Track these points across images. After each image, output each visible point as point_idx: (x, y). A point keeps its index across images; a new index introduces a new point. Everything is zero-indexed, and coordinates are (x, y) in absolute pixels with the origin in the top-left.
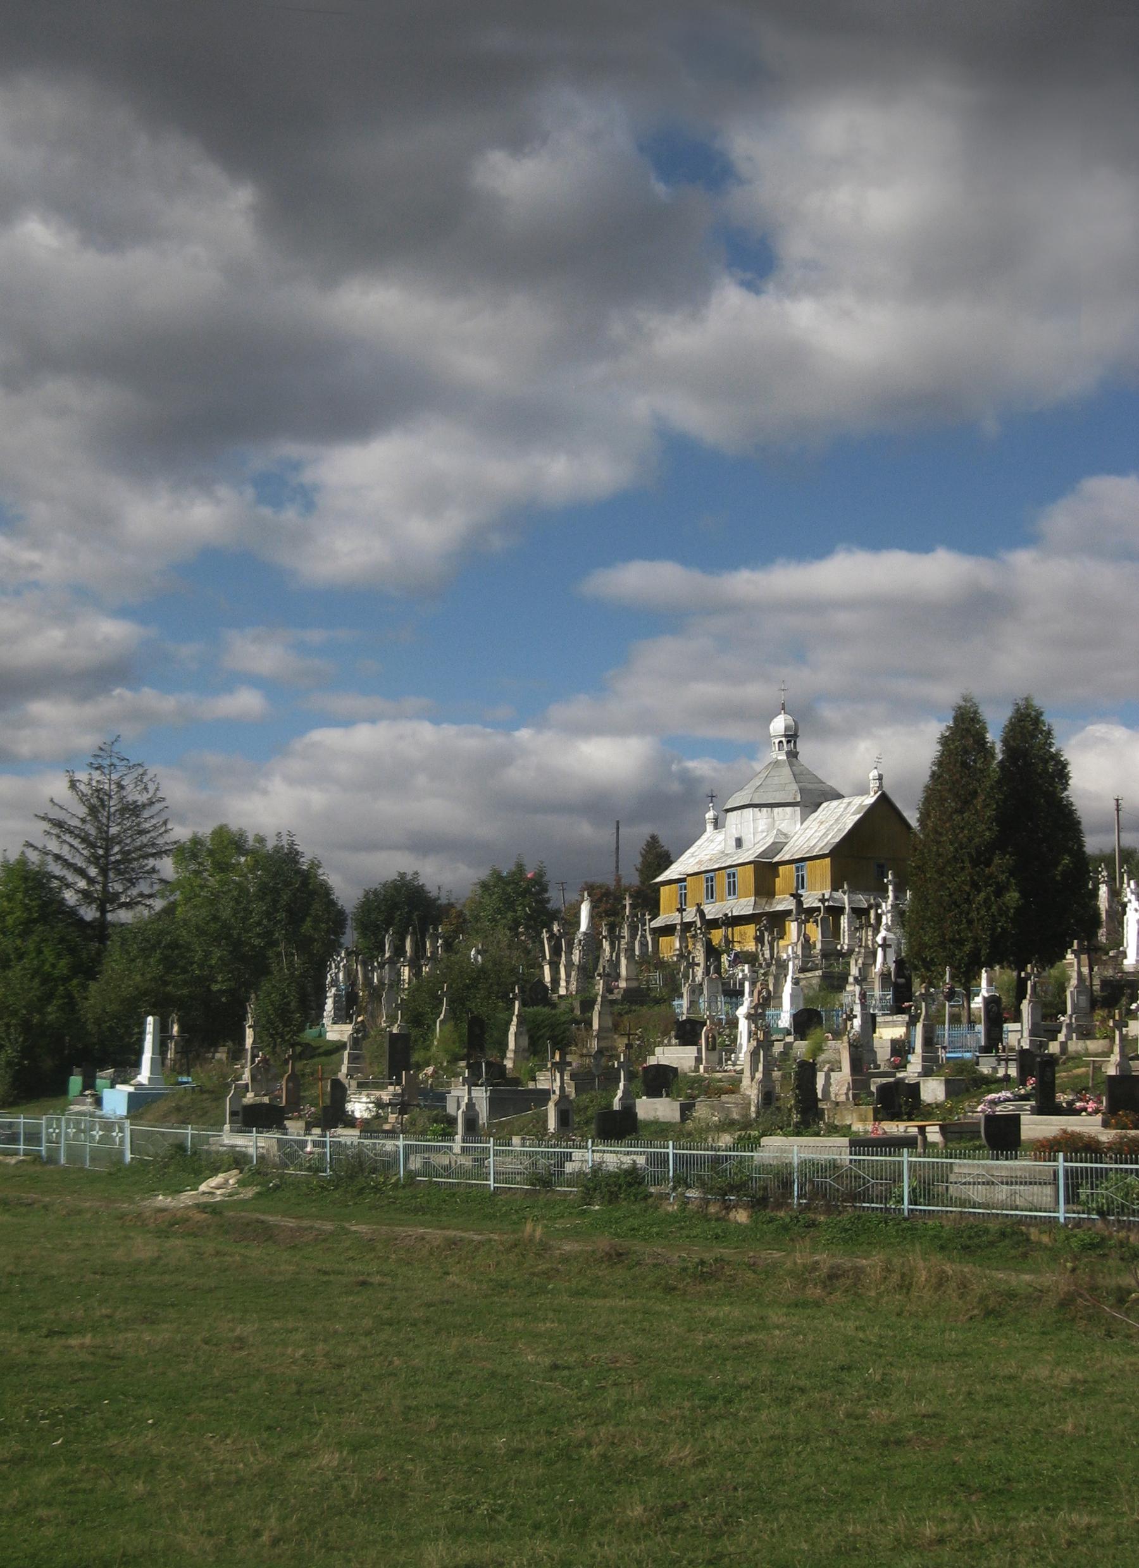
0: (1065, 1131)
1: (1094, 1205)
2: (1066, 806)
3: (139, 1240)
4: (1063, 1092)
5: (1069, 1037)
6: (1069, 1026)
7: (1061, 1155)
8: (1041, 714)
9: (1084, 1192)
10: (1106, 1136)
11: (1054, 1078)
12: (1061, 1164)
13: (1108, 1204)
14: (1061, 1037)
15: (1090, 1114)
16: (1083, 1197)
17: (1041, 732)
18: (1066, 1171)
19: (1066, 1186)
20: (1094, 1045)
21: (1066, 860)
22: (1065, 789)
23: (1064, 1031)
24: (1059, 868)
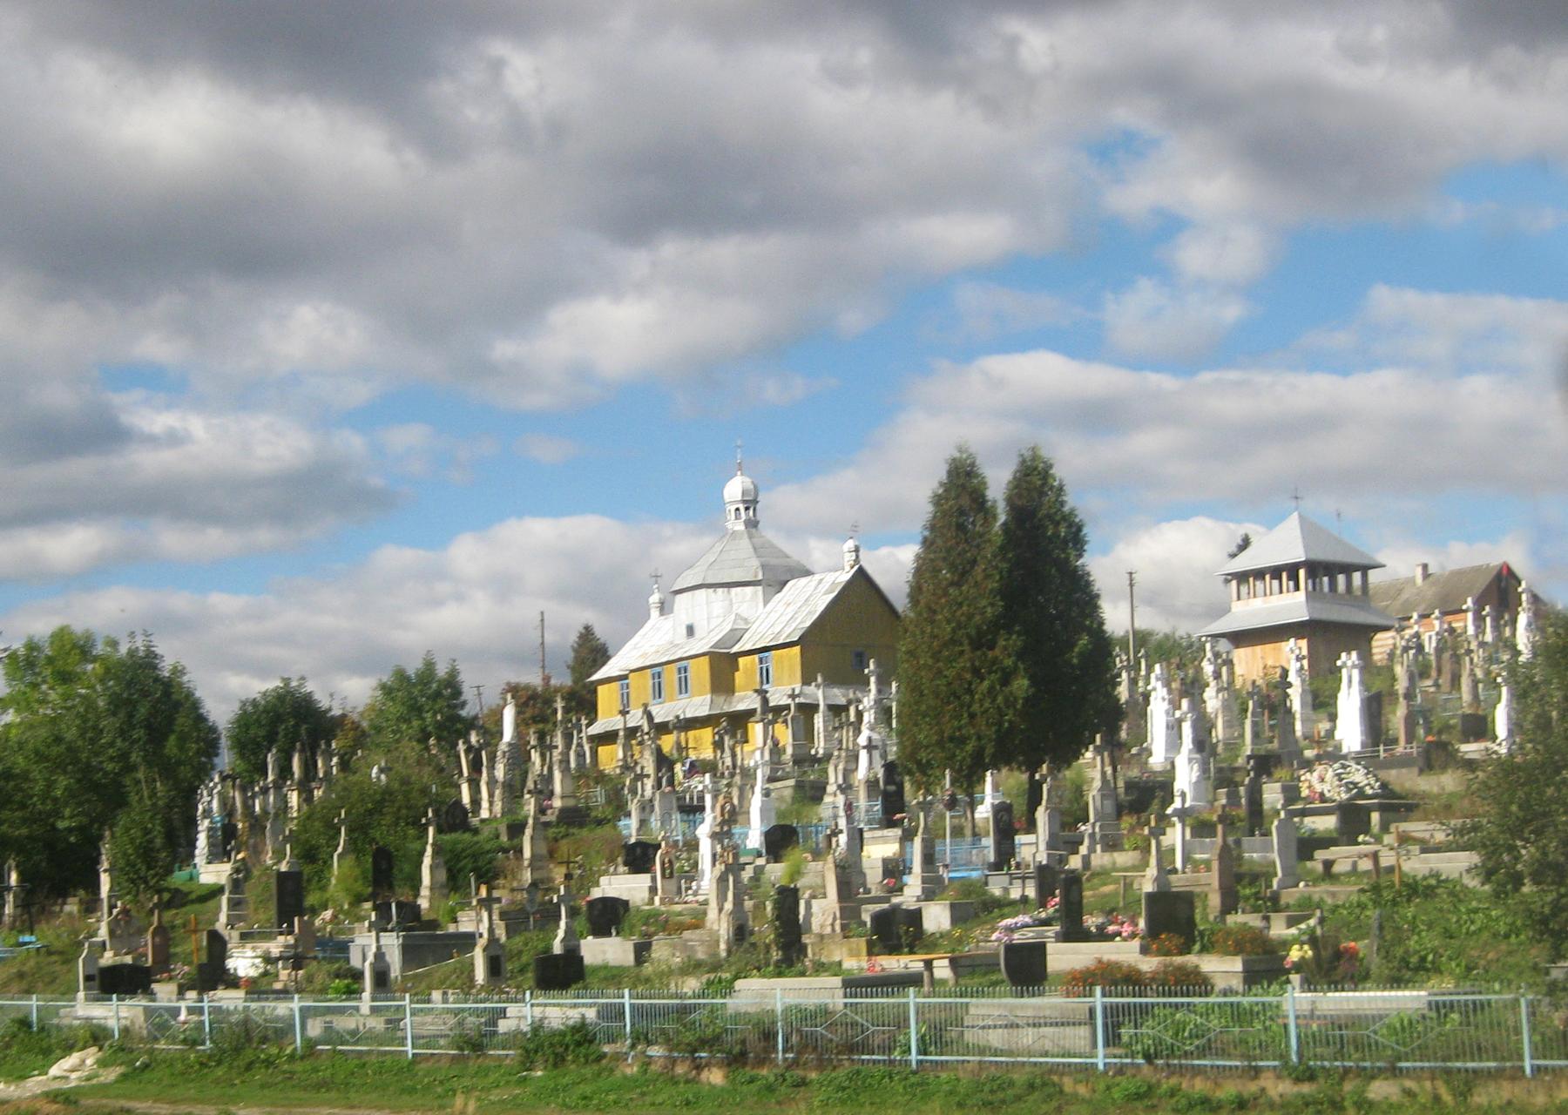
0: (1100, 961)
1: (1139, 1047)
5: (1092, 850)
7: (1098, 990)
8: (1051, 466)
9: (1126, 1032)
10: (1149, 964)
12: (1098, 999)
14: (1083, 850)
15: (1125, 940)
16: (1125, 1039)
17: (1052, 488)
18: (917, 1004)
19: (1105, 1025)
20: (1124, 858)
21: (1084, 640)
22: (1080, 556)
23: (1086, 842)
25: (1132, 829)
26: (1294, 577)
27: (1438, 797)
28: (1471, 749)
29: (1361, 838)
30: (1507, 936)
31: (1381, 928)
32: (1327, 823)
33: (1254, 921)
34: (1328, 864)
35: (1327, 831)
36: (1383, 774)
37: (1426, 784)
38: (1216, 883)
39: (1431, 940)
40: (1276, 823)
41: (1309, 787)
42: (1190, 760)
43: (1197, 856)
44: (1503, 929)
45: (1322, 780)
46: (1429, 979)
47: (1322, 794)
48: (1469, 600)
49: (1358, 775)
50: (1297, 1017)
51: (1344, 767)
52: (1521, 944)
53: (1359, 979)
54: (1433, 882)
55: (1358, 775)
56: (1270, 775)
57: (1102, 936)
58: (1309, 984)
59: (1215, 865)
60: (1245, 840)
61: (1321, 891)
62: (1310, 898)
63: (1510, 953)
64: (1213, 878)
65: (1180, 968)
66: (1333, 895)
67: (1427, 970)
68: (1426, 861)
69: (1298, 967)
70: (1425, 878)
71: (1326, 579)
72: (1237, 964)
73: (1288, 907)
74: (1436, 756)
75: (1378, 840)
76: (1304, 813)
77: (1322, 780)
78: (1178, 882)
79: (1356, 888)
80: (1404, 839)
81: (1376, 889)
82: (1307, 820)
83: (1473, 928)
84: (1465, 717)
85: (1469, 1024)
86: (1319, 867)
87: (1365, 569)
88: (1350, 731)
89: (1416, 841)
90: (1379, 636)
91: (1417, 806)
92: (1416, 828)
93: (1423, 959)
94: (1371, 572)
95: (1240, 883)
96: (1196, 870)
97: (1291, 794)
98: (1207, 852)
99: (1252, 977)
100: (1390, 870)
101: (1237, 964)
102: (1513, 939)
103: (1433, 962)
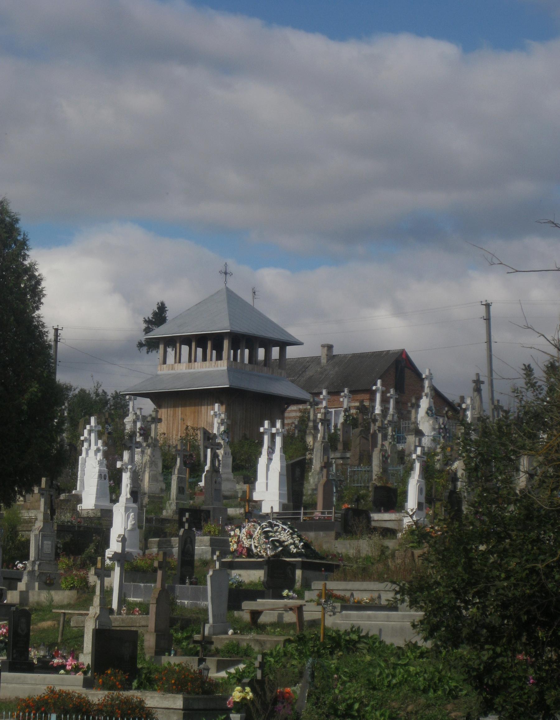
0: (52, 691)
3: (528, 591)
5: (29, 586)
6: (31, 573)
8: (17, 221)
14: (22, 586)
15: (68, 672)
17: (16, 241)
20: (61, 596)
21: (35, 388)
22: (38, 308)
23: (25, 579)
24: (26, 397)
25: (69, 569)
28: (381, 518)
29: (285, 593)
31: (313, 676)
32: (255, 576)
33: (192, 663)
34: (255, 614)
35: (251, 583)
36: (311, 536)
37: (344, 547)
38: (152, 625)
40: (211, 573)
41: (238, 542)
42: (127, 509)
43: (131, 599)
44: (421, 682)
45: (250, 536)
47: (249, 550)
48: (379, 382)
49: (284, 535)
52: (438, 698)
54: (354, 637)
55: (284, 535)
56: (199, 528)
57: (45, 667)
59: (153, 609)
60: (178, 586)
61: (248, 639)
62: (238, 645)
63: (428, 706)
64: (151, 620)
65: (127, 701)
68: (347, 617)
70: (347, 633)
71: (247, 351)
73: (217, 652)
74: (353, 522)
75: (301, 596)
76: (232, 566)
77: (250, 536)
78: (118, 621)
79: (282, 639)
80: (329, 596)
81: (301, 640)
82: (235, 573)
83: (394, 681)
86: (246, 617)
87: (283, 345)
88: (268, 490)
89: (342, 599)
90: (293, 408)
91: (338, 566)
92: (336, 586)
93: (350, 707)
94: (289, 348)
95: (176, 627)
97: (220, 544)
98: (146, 594)
100: (314, 623)
102: (431, 694)
103: (358, 711)
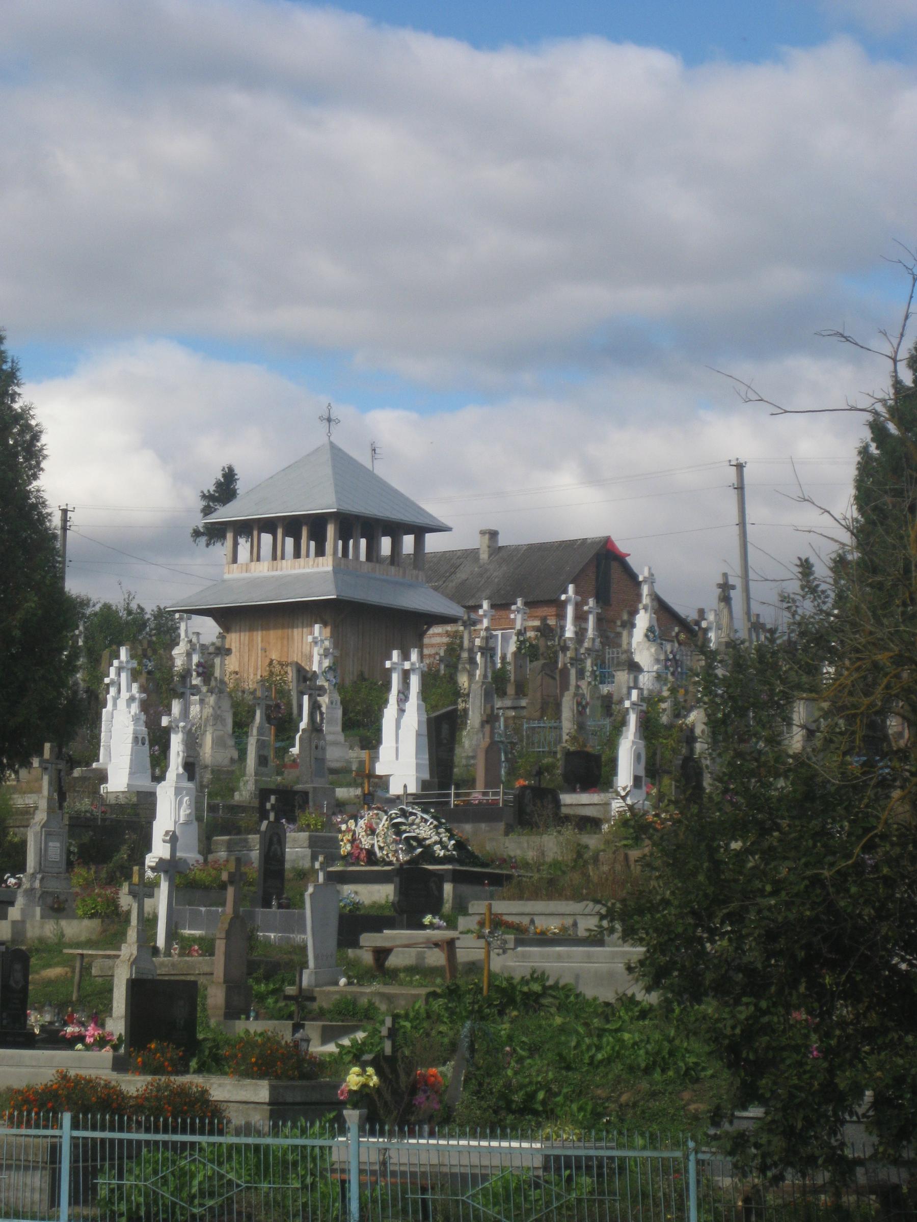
0: (64, 1077)
1: (124, 1207)
2: (34, 506)
4: (40, 1010)
7: (67, 1118)
9: (104, 1183)
10: (134, 1084)
11: (27, 982)
12: (66, 1131)
13: (147, 1205)
15: (88, 1047)
16: (103, 1193)
18: (74, 1140)
19: (74, 1171)
22: (35, 477)
23: (20, 901)
26: (319, 537)
27: (538, 866)
29: (427, 919)
30: (648, 1071)
33: (284, 1031)
34: (381, 954)
35: (374, 905)
37: (519, 847)
39: (540, 1070)
42: (178, 791)
43: (187, 932)
45: (371, 831)
46: (539, 1125)
47: (370, 853)
50: (361, 1172)
51: (404, 813)
53: (443, 1121)
54: (536, 987)
55: (425, 829)
56: (292, 820)
57: (53, 1039)
58: (373, 1123)
59: (220, 946)
62: (355, 1003)
63: (653, 1095)
65: (182, 1092)
66: (389, 998)
67: (535, 1113)
69: (361, 1097)
71: (363, 542)
72: (261, 1091)
74: (532, 808)
77: (371, 831)
78: (168, 965)
79: (423, 991)
81: (453, 992)
83: (599, 1056)
84: (568, 754)
85: (602, 1193)
86: (367, 958)
87: (420, 531)
88: (400, 758)
90: (436, 630)
91: (509, 877)
93: (531, 1096)
94: (428, 536)
96: (186, 950)
97: (324, 845)
98: (209, 923)
99: (280, 1111)
100: (473, 967)
101: (261, 1091)
102: (657, 1076)
103: (544, 1103)
